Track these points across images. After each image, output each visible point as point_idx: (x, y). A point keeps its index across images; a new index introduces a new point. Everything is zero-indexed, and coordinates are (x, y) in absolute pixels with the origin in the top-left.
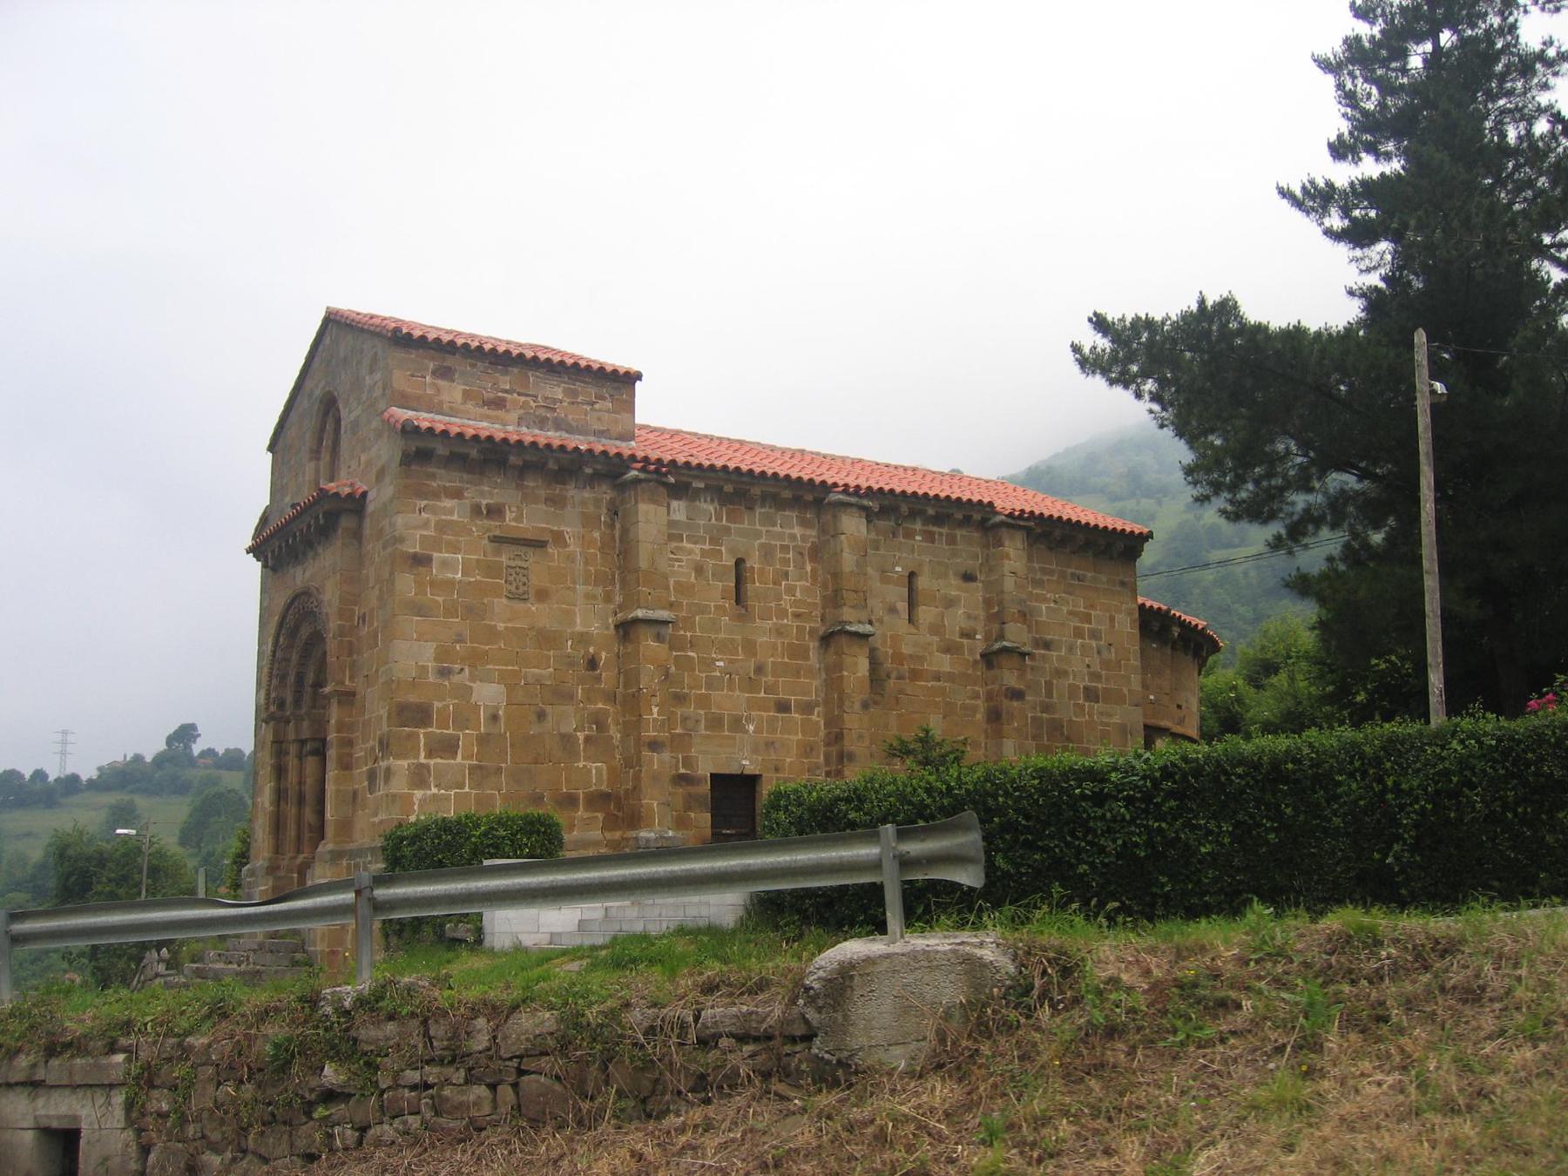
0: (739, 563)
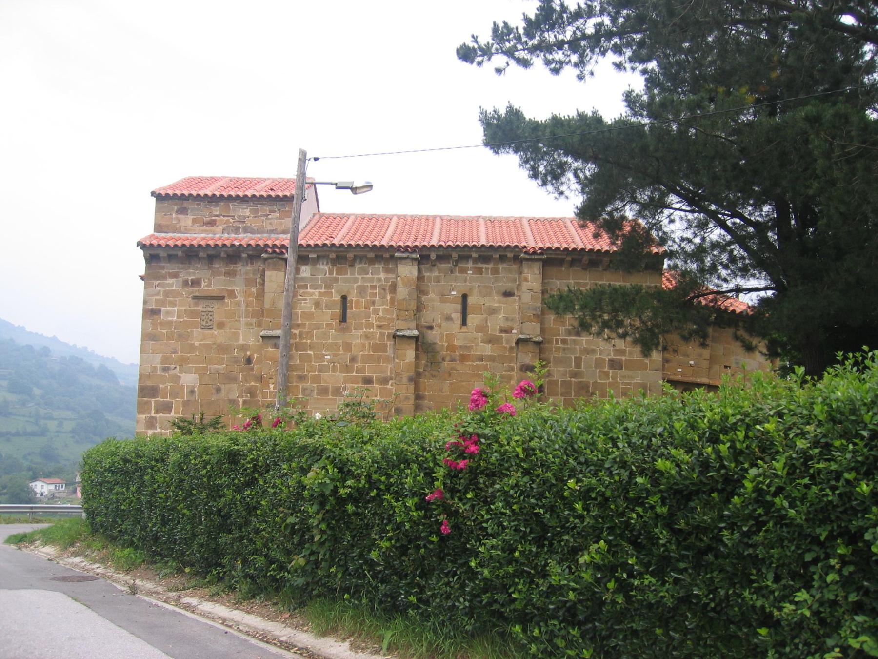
0: (344, 298)
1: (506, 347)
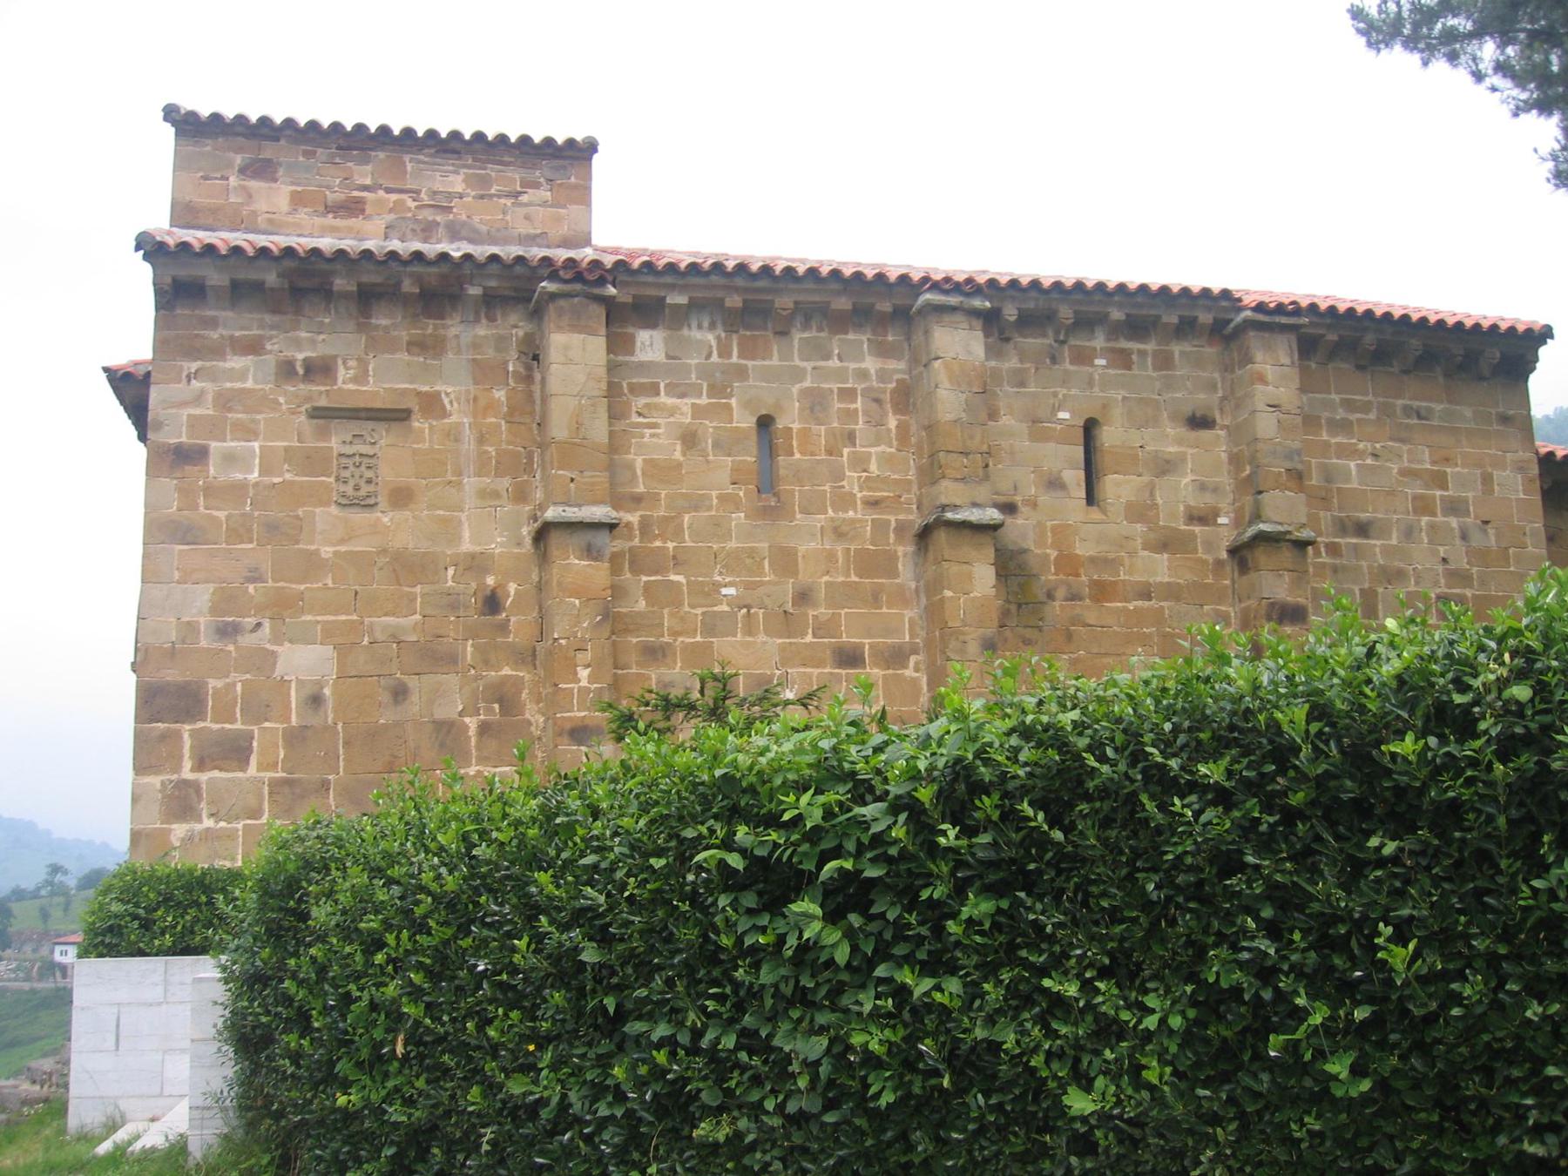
0: (765, 423)
1: (1204, 562)
